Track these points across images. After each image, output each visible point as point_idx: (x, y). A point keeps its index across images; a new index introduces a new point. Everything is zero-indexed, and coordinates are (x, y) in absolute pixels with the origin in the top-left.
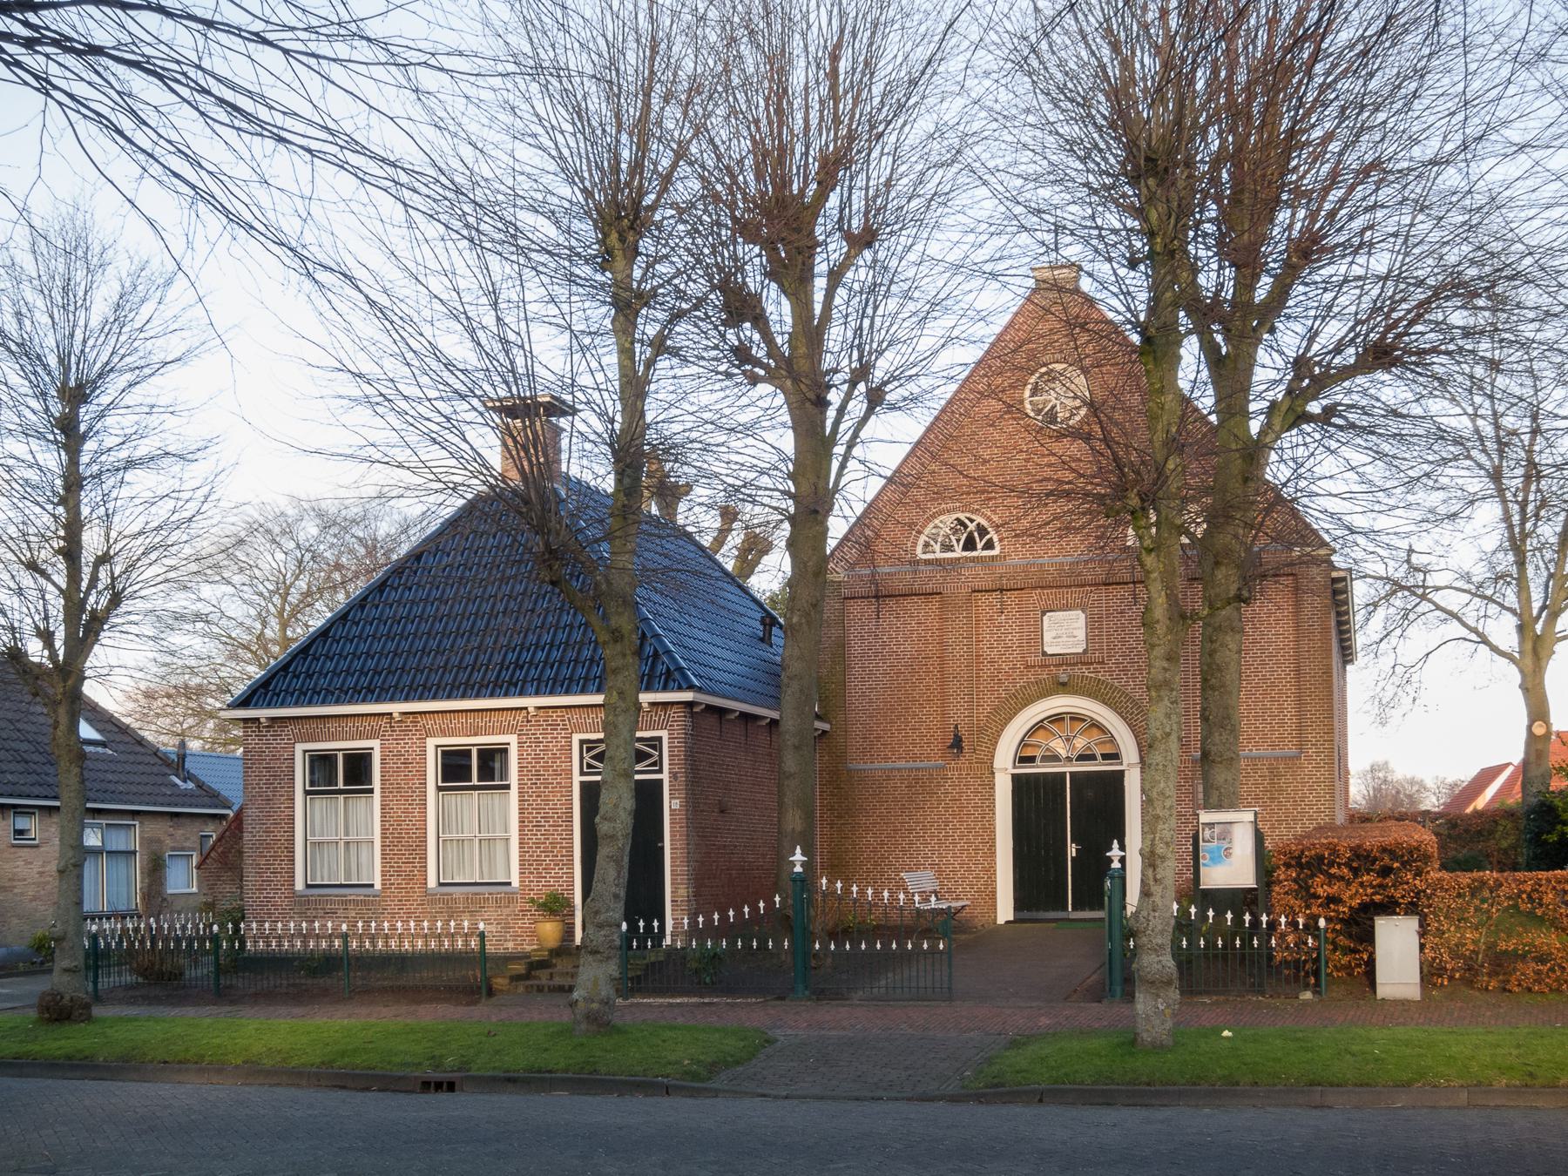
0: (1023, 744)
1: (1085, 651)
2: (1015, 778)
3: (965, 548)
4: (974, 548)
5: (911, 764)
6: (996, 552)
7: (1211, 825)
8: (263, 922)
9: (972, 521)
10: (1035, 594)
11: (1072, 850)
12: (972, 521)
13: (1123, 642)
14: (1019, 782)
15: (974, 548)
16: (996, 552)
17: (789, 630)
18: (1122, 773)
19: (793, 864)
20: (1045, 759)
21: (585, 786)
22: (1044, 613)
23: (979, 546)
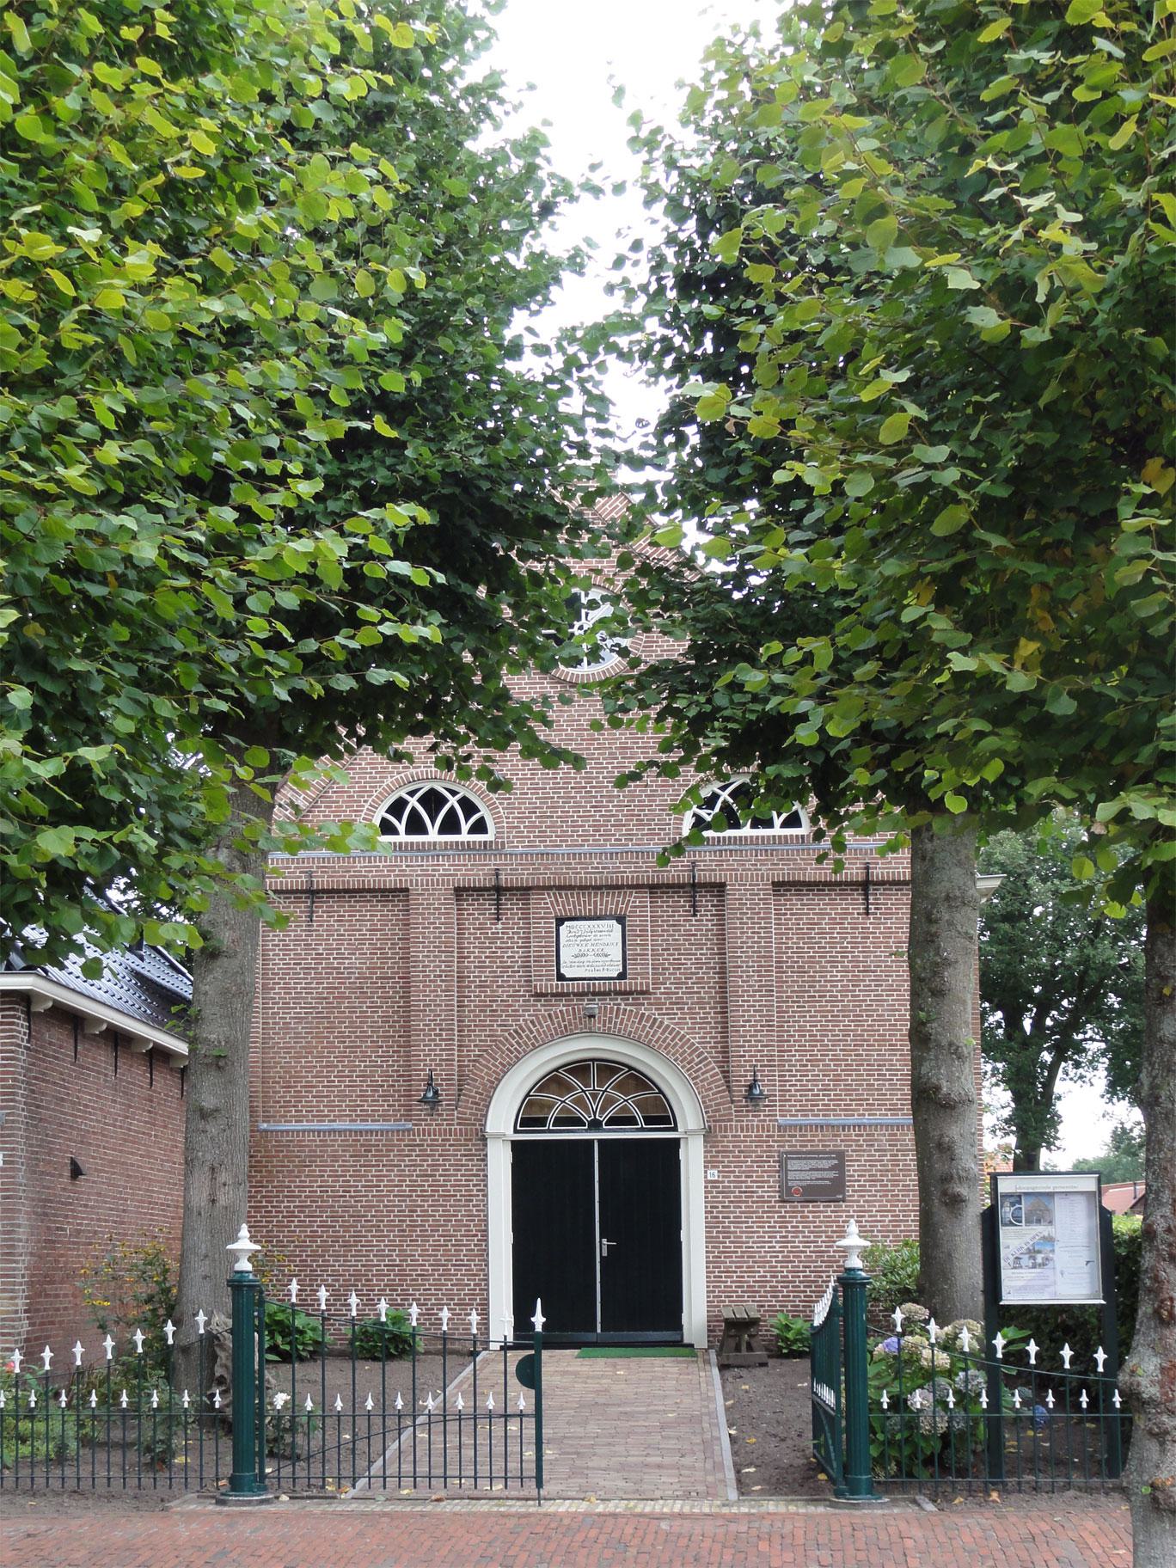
0: (529, 1103)
1: (622, 976)
2: (516, 1146)
3: (442, 831)
4: (457, 831)
5: (359, 1126)
6: (489, 837)
7: (1017, 1198)
8: (135, 1407)
9: (454, 793)
10: (548, 898)
11: (602, 1246)
12: (454, 793)
13: (678, 965)
14: (519, 1150)
15: (457, 831)
16: (489, 837)
17: (672, 697)
18: (676, 1143)
19: (234, 1256)
20: (558, 1122)
21: (754, 826)
22: (560, 921)
23: (465, 827)
